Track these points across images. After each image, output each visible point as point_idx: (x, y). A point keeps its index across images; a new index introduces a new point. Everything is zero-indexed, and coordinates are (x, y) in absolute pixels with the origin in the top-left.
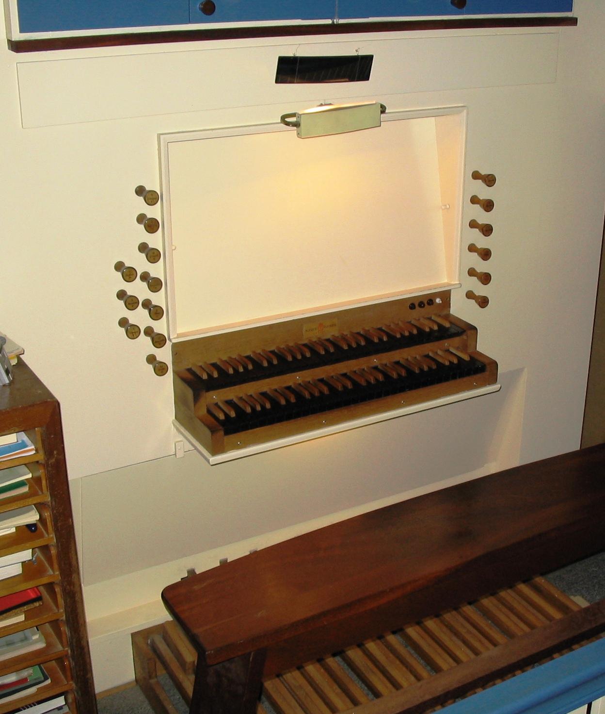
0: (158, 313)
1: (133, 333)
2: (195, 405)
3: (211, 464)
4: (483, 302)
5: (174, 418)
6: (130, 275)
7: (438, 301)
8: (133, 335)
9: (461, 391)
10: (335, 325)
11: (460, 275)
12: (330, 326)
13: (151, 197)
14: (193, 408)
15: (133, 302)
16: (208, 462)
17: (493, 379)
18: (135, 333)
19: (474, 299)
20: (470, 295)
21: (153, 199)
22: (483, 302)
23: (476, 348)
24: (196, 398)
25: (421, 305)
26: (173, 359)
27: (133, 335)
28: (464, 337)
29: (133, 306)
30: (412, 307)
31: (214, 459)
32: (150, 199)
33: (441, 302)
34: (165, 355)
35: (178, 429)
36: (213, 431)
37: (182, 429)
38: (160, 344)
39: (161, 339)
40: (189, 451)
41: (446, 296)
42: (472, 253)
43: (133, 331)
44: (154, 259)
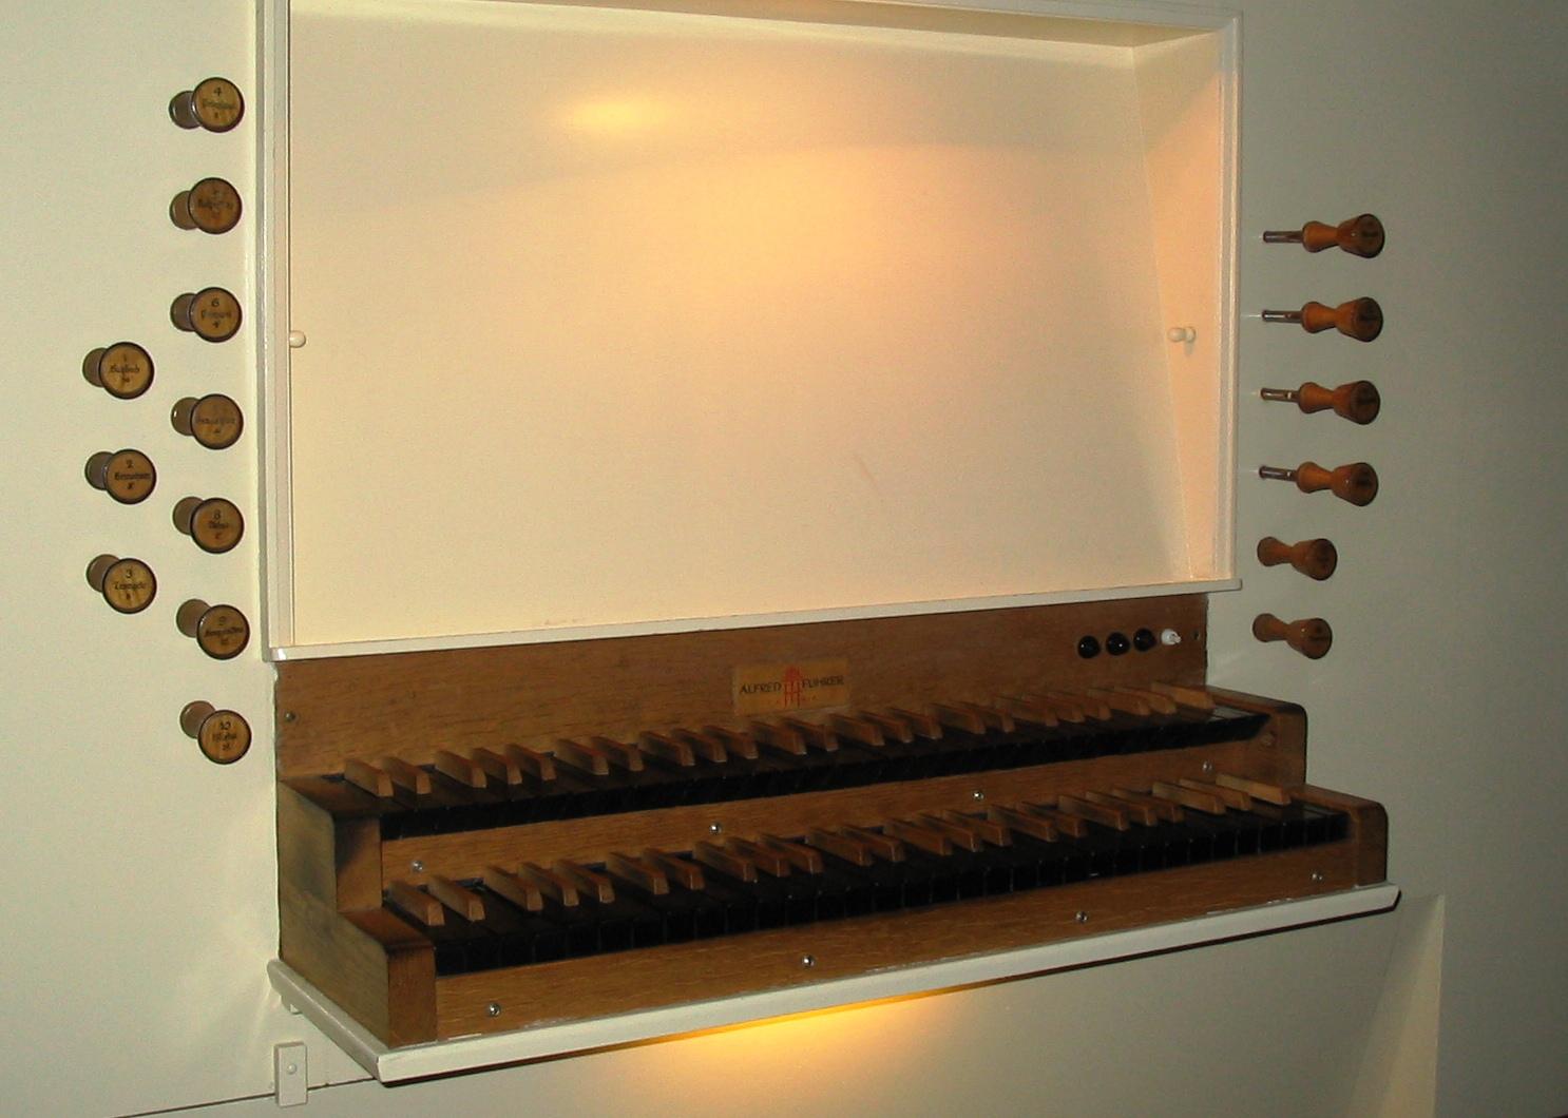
0: (224, 526)
1: (125, 587)
2: (338, 871)
3: (384, 1080)
4: (1315, 639)
5: (276, 956)
6: (125, 370)
7: (1169, 637)
8: (128, 596)
9: (1272, 898)
10: (840, 680)
11: (1235, 537)
12: (825, 682)
13: (215, 98)
14: (332, 884)
15: (131, 472)
16: (371, 1067)
17: (1376, 873)
18: (135, 587)
19: (1284, 639)
20: (1266, 628)
21: (222, 106)
22: (1315, 639)
23: (1305, 780)
24: (344, 852)
25: (1117, 645)
26: (278, 735)
27: (128, 596)
28: (1265, 739)
29: (227, 747)
30: (1089, 648)
31: (399, 1063)
32: (214, 105)
33: (1178, 640)
34: (257, 707)
35: (288, 998)
36: (395, 950)
37: (309, 996)
38: (224, 643)
39: (229, 625)
40: (327, 1085)
41: (1189, 610)
42: (1353, 214)
43: (129, 581)
44: (216, 325)
